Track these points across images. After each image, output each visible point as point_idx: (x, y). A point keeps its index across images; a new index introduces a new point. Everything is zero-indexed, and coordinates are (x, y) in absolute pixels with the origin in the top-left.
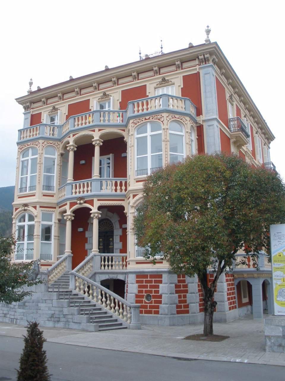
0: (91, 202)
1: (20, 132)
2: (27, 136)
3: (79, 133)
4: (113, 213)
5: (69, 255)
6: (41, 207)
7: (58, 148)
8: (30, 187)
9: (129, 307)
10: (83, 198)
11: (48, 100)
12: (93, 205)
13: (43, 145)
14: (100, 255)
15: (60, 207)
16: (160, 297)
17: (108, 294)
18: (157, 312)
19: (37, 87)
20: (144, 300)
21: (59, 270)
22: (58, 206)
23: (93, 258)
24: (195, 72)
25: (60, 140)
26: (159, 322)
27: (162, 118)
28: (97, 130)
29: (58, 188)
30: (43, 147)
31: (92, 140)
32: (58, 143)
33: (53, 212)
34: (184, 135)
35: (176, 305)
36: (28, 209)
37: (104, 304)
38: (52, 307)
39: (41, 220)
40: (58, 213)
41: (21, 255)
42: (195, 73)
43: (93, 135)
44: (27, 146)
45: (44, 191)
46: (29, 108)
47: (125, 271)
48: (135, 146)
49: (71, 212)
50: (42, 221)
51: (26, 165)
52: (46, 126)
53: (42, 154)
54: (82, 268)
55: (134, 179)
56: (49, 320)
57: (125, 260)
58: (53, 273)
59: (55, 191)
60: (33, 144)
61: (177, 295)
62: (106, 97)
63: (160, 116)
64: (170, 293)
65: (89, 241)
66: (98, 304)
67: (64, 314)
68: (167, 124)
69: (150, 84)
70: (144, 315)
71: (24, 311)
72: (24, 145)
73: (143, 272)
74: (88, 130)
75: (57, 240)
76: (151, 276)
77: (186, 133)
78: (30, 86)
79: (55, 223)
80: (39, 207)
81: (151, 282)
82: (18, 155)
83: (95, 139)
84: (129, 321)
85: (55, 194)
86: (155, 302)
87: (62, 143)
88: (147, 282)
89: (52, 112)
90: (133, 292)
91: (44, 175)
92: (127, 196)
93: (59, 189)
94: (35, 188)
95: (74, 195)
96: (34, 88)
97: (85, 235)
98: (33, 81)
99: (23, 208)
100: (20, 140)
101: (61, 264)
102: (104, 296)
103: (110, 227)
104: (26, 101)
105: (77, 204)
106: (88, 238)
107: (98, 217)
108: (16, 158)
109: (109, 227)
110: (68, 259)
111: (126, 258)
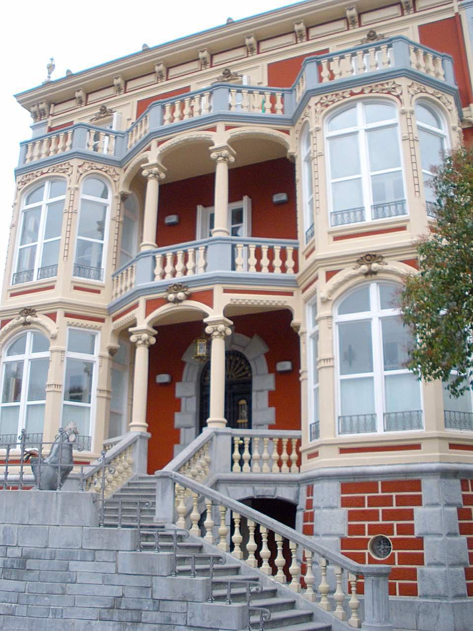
0: (207, 297)
1: (24, 147)
2: (40, 153)
3: (176, 136)
4: (250, 335)
5: (142, 433)
6: (67, 315)
7: (115, 181)
8: (42, 269)
9: (353, 573)
10: (185, 287)
11: (90, 96)
12: (210, 304)
13: (81, 171)
14: (231, 434)
15: (114, 319)
16: (419, 543)
17: (279, 533)
18: (411, 591)
19: (66, 70)
20: (369, 554)
21: (122, 468)
22: (110, 315)
23: (212, 439)
24: (450, 15)
25: (120, 164)
26: (421, 619)
27: (397, 90)
28: (220, 126)
29: (112, 272)
30: (79, 174)
31: (211, 148)
32: (114, 170)
33: (96, 331)
34: (447, 134)
35: (465, 569)
36: (35, 319)
37: (265, 565)
38: (117, 572)
39: (65, 348)
40: (110, 333)
41: (9, 436)
42: (445, 19)
43: (212, 139)
44: (39, 174)
45: (77, 278)
46: (44, 114)
47: (298, 476)
48: (326, 155)
49: (149, 323)
50: (69, 350)
51: (32, 230)
52: (89, 131)
53: (76, 191)
54: (187, 465)
55: (329, 233)
56: (103, 617)
57: (294, 447)
58: (95, 484)
59: (105, 279)
60: (54, 170)
61: (464, 538)
62: (229, 78)
63: (390, 84)
64: (447, 531)
65: (186, 406)
66: (246, 567)
67: (156, 596)
68: (411, 103)
69: (337, 46)
70: (398, 598)
71: (20, 585)
72: (30, 175)
73: (364, 475)
74: (200, 128)
75: (104, 400)
76: (387, 486)
77: (452, 132)
78: (50, 73)
79: (101, 357)
80: (63, 314)
81: (387, 501)
82: (16, 198)
83: (217, 145)
84: (354, 620)
85: (103, 287)
86: (403, 559)
87: (125, 170)
88: (373, 502)
89: (97, 119)
90: (333, 531)
91: (78, 240)
92: (300, 284)
93: (113, 276)
94: (54, 270)
95: (158, 280)
96: (59, 74)
97: (174, 391)
98: (55, 62)
99: (22, 318)
100: (25, 163)
101: (120, 458)
102: (265, 540)
103: (241, 373)
104: (39, 100)
105: (166, 301)
106: (183, 400)
107: (223, 334)
108: (12, 204)
109: (238, 372)
110: (138, 444)
111: (299, 443)
